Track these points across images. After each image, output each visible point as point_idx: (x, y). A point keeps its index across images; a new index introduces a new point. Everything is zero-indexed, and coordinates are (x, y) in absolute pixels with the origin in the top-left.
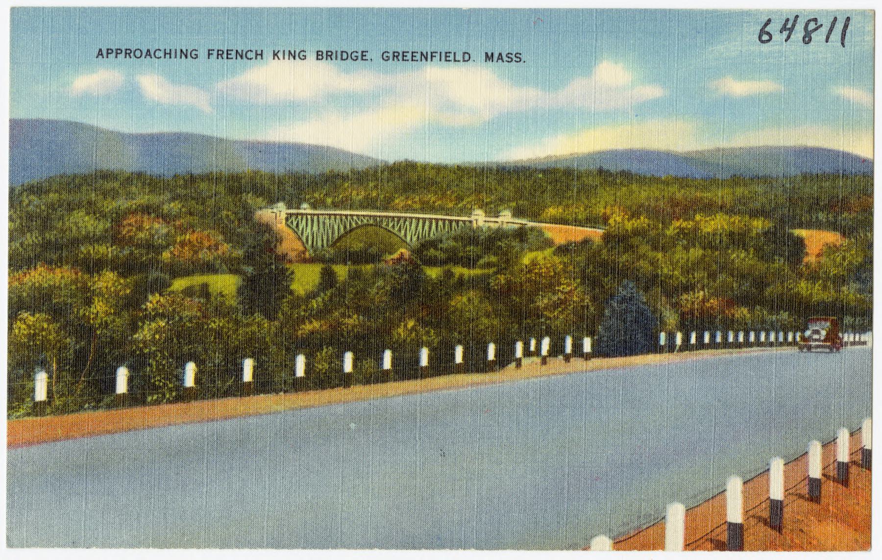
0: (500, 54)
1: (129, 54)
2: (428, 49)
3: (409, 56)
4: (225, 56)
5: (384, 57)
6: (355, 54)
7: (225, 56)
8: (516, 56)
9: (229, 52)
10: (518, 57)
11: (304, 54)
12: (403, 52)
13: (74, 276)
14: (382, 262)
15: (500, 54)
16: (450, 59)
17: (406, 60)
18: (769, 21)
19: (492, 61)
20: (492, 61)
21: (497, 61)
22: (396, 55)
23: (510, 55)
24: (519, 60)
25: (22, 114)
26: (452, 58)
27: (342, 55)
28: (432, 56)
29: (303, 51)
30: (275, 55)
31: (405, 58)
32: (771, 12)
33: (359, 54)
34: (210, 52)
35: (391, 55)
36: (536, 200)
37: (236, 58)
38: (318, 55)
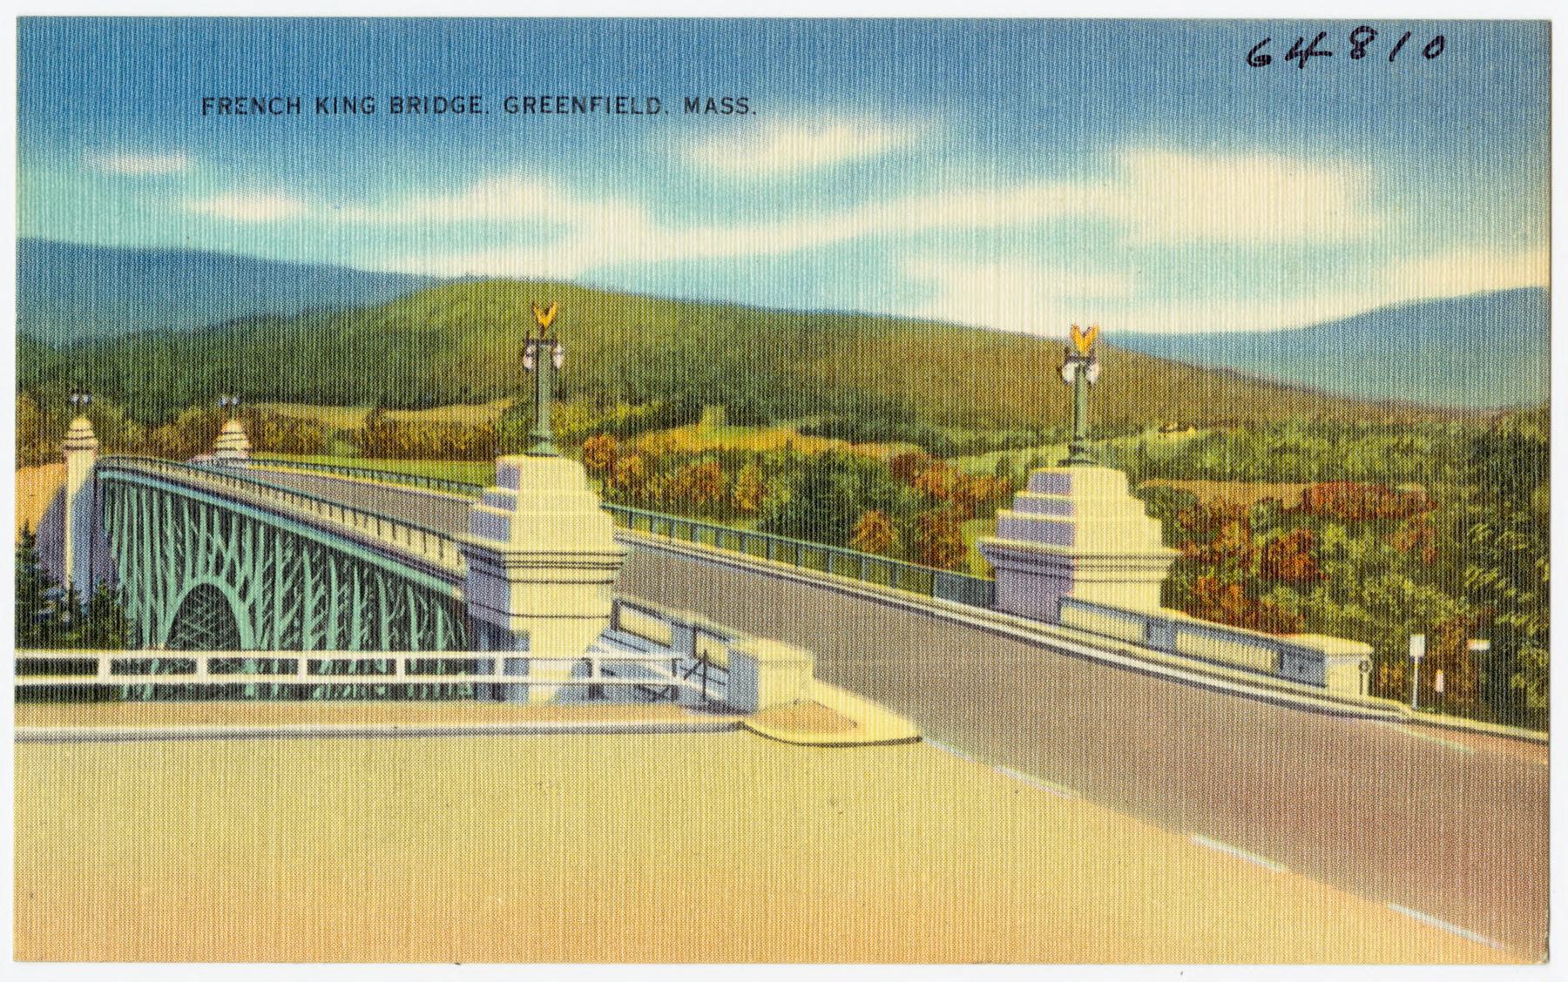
0: (711, 100)
1: (415, 106)
2: (585, 93)
3: (553, 103)
4: (537, 107)
5: (456, 106)
6: (513, 102)
7: (537, 107)
8: (731, 107)
9: (620, 102)
10: (727, 105)
11: (371, 103)
12: (543, 98)
13: (83, 603)
14: (544, 444)
15: (711, 100)
16: (625, 109)
17: (623, 112)
18: (1322, 35)
19: (698, 111)
20: (698, 111)
21: (706, 113)
22: (529, 104)
23: (726, 109)
24: (728, 110)
25: (32, 232)
26: (627, 108)
27: (649, 106)
28: (593, 105)
29: (369, 98)
30: (396, 105)
31: (545, 108)
32: (1270, 23)
33: (467, 103)
34: (561, 101)
35: (520, 103)
36: (1104, 498)
37: (574, 111)
38: (393, 105)
